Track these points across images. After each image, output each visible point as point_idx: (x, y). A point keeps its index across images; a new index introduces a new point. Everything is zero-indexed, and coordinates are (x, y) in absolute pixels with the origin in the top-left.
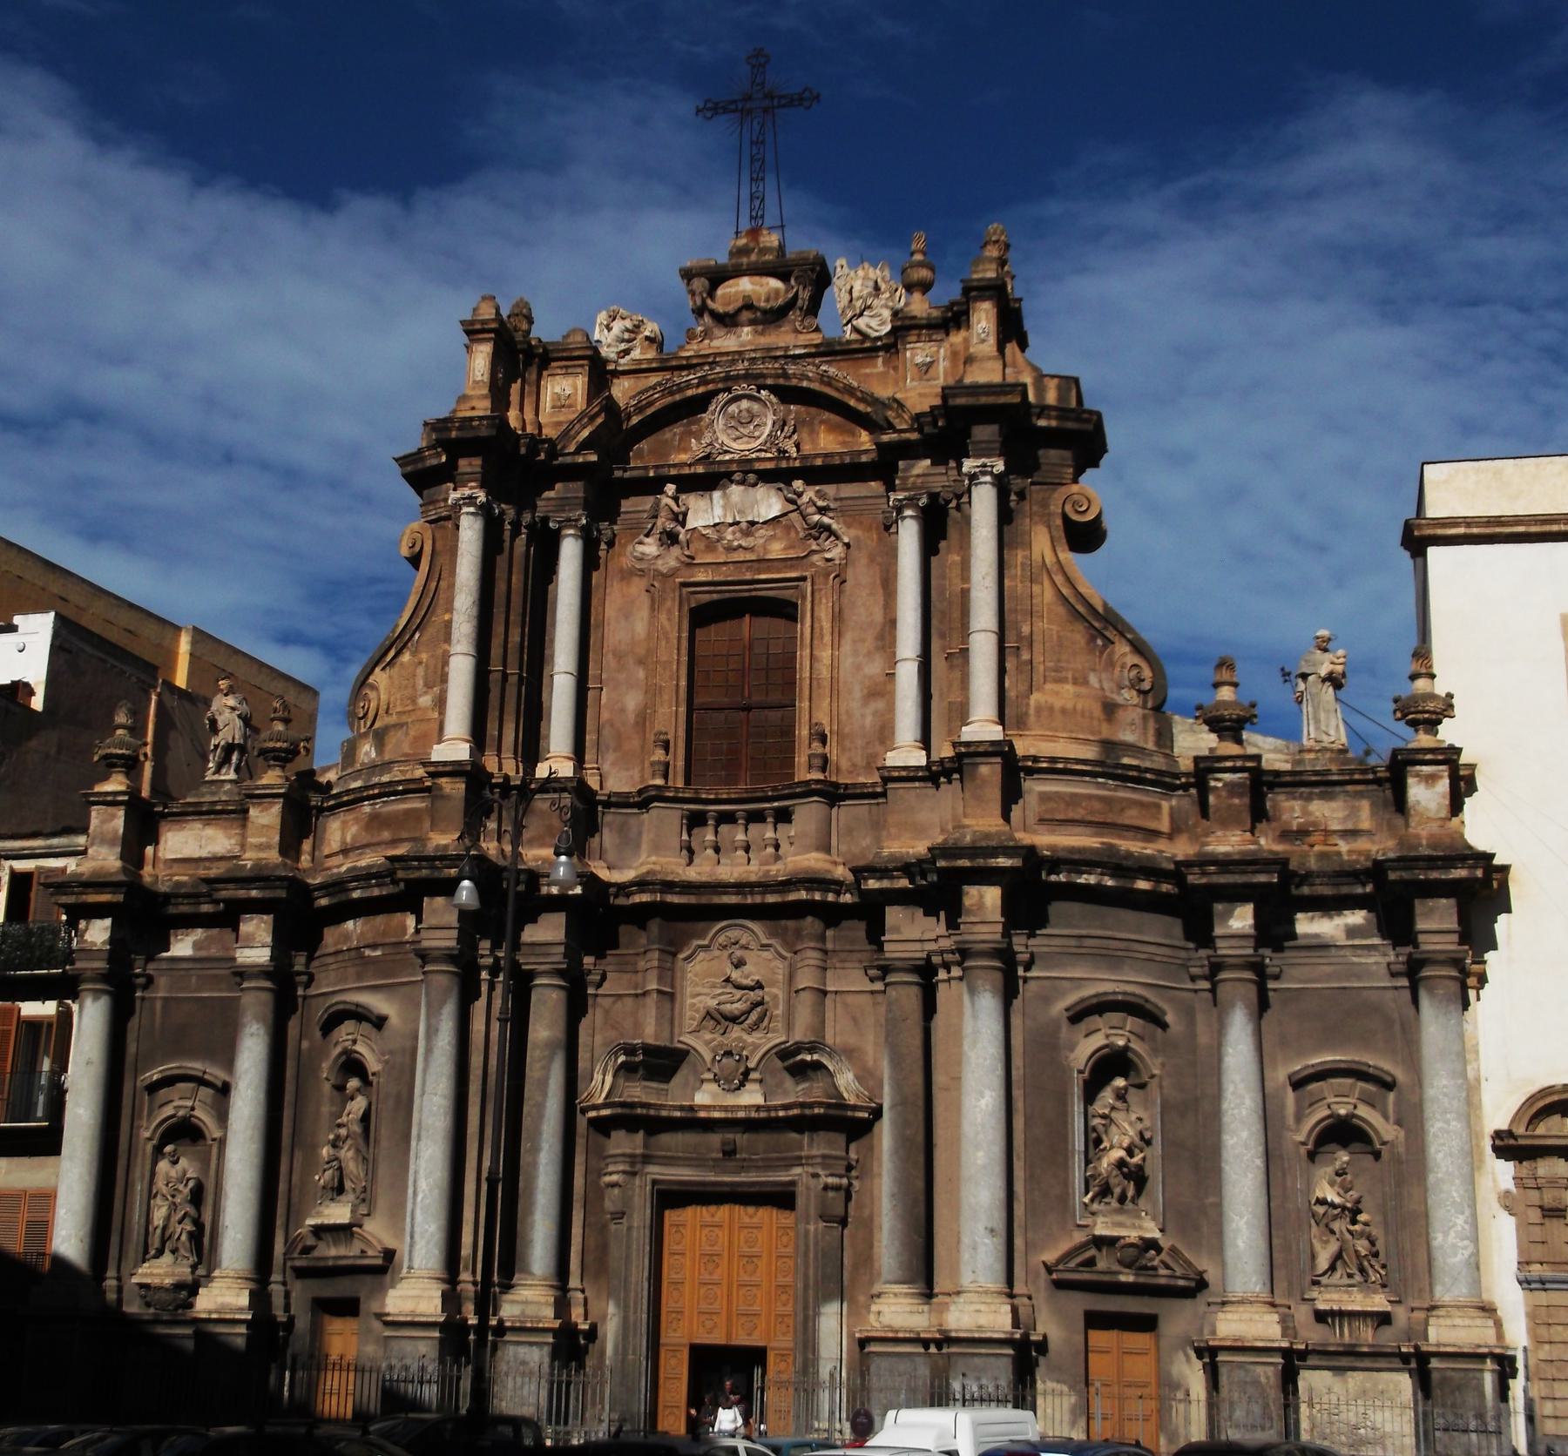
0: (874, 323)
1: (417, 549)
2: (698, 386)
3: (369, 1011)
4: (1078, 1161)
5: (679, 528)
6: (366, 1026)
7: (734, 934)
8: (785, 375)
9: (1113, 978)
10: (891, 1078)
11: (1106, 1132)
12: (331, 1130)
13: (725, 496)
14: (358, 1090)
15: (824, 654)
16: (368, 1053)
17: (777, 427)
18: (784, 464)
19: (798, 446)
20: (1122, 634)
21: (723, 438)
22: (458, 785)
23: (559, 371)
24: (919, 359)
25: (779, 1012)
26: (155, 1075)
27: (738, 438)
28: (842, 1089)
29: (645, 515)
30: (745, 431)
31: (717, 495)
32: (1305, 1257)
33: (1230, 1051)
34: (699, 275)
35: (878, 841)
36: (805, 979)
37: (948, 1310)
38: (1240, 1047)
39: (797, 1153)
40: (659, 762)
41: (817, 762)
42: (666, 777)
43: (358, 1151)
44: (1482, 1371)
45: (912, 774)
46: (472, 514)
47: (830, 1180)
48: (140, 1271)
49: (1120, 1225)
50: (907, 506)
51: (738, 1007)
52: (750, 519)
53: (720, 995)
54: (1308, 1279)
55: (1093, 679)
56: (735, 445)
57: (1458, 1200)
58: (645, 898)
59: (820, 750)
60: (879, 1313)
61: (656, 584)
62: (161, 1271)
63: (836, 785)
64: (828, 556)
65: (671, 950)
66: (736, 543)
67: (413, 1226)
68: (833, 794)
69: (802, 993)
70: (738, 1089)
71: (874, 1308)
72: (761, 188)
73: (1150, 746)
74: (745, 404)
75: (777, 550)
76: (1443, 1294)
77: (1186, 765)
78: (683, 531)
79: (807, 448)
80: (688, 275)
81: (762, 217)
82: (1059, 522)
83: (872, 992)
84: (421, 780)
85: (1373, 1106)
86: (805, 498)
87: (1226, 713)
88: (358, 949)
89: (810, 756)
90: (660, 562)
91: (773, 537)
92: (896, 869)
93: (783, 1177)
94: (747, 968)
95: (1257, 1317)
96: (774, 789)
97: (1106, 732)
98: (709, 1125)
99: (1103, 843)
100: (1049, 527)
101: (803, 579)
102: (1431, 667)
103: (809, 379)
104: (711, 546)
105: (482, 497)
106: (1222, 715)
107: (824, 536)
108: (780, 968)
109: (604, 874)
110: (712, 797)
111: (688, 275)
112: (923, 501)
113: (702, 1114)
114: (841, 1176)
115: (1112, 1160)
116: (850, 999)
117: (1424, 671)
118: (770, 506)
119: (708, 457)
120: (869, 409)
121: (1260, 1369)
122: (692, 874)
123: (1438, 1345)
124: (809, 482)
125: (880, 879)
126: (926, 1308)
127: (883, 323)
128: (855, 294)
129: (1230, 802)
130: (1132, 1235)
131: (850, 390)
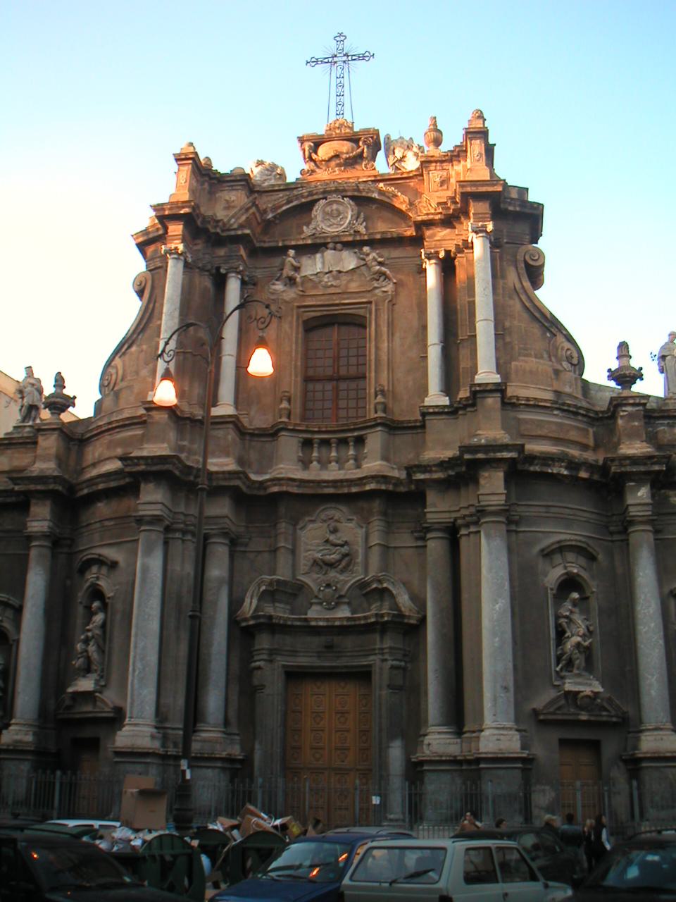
1: (143, 284)
2: (308, 196)
3: (107, 558)
4: (553, 643)
5: (296, 275)
6: (104, 570)
7: (331, 513)
8: (358, 190)
9: (568, 532)
11: (568, 627)
12: (83, 633)
13: (323, 257)
17: (354, 218)
18: (358, 238)
20: (560, 331)
21: (322, 225)
22: (163, 416)
23: (227, 188)
25: (360, 559)
27: (331, 225)
28: (401, 605)
31: (318, 256)
34: (308, 140)
35: (418, 455)
38: (647, 572)
39: (373, 647)
40: (285, 409)
41: (380, 407)
42: (289, 417)
43: (99, 646)
45: (441, 410)
49: (580, 684)
51: (335, 557)
52: (338, 269)
56: (329, 229)
58: (276, 489)
59: (383, 400)
60: (429, 744)
61: (282, 307)
63: (393, 421)
65: (294, 522)
66: (329, 284)
68: (393, 427)
69: (373, 548)
70: (333, 608)
73: (580, 396)
74: (335, 206)
75: (354, 287)
78: (298, 276)
80: (302, 140)
81: (343, 114)
82: (523, 265)
83: (417, 547)
84: (140, 417)
86: (371, 257)
87: (627, 372)
90: (284, 294)
91: (352, 280)
92: (435, 465)
93: (364, 662)
94: (339, 535)
95: (665, 738)
97: (556, 387)
98: (316, 631)
100: (517, 268)
101: (370, 303)
104: (315, 286)
106: (625, 374)
107: (382, 279)
108: (361, 532)
109: (253, 477)
111: (302, 140)
113: (313, 623)
114: (401, 661)
115: (573, 644)
116: (403, 551)
119: (314, 234)
125: (424, 472)
126: (459, 740)
130: (587, 690)
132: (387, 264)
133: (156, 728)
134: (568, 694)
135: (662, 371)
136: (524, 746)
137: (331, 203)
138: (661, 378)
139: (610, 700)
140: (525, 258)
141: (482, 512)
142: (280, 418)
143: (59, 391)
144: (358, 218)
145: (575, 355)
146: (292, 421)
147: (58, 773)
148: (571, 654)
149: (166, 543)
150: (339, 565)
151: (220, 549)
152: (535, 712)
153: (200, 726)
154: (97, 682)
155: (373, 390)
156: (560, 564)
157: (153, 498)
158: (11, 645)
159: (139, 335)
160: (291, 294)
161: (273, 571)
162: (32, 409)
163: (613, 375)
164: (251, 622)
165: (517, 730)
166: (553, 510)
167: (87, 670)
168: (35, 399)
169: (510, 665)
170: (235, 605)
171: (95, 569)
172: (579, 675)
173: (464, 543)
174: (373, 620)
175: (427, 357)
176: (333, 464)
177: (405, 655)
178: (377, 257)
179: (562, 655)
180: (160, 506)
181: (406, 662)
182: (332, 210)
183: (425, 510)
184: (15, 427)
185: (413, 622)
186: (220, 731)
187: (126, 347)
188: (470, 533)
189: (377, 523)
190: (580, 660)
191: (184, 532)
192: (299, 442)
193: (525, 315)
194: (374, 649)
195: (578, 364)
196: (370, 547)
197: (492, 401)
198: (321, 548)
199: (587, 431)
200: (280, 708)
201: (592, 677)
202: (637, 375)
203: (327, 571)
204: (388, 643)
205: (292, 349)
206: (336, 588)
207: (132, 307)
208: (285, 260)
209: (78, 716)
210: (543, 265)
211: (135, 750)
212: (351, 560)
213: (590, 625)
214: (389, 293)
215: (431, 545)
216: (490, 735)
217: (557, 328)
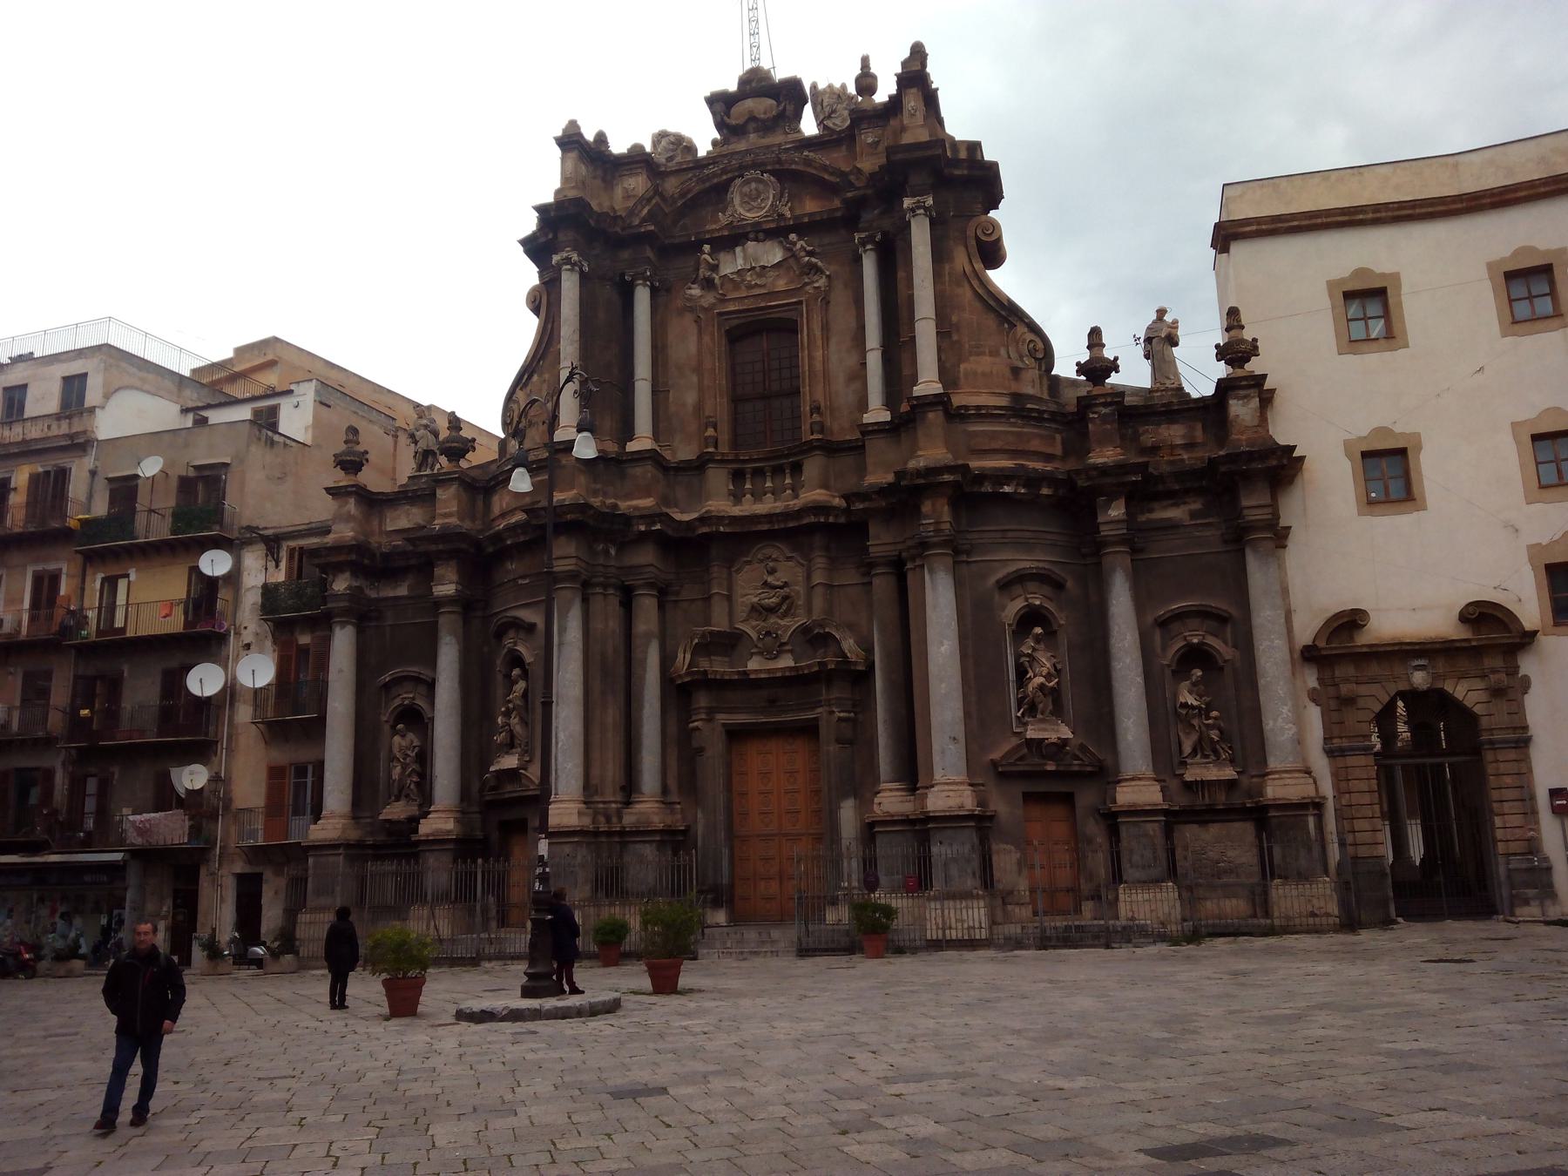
0: (838, 122)
2: (721, 174)
5: (714, 275)
6: (522, 635)
7: (768, 551)
8: (779, 161)
10: (878, 640)
13: (744, 251)
14: (519, 676)
15: (818, 354)
16: (526, 652)
19: (790, 209)
21: (741, 210)
23: (626, 173)
24: (870, 140)
26: (386, 678)
29: (691, 269)
30: (755, 204)
31: (738, 250)
32: (1174, 747)
33: (1114, 602)
36: (818, 578)
37: (927, 797)
41: (816, 428)
42: (716, 447)
43: (521, 719)
44: (1307, 815)
45: (881, 428)
46: (569, 270)
47: (842, 715)
48: (384, 811)
49: (1045, 730)
50: (868, 243)
53: (760, 594)
54: (1176, 760)
55: (1003, 352)
56: (748, 215)
57: (1282, 695)
58: (705, 530)
59: (818, 419)
62: (398, 810)
64: (816, 285)
66: (753, 283)
67: (556, 765)
68: (832, 449)
70: (775, 658)
71: (876, 801)
72: (757, 40)
73: (1046, 396)
74: (753, 185)
75: (781, 285)
76: (1273, 763)
77: (1072, 408)
79: (798, 212)
81: (759, 59)
82: (973, 242)
83: (863, 584)
85: (1216, 636)
86: (798, 246)
87: (1098, 365)
88: (514, 579)
89: (811, 424)
90: (703, 300)
96: (789, 448)
97: (1015, 387)
99: (1015, 464)
101: (800, 303)
102: (1240, 321)
103: (796, 163)
104: (736, 286)
105: (575, 257)
108: (800, 573)
109: (678, 517)
110: (747, 458)
112: (878, 238)
113: (752, 676)
114: (849, 712)
115: (1035, 685)
117: (1236, 324)
118: (775, 255)
120: (838, 180)
121: (1149, 826)
122: (736, 511)
123: (1274, 800)
124: (800, 237)
125: (863, 501)
126: (912, 797)
127: (844, 120)
128: (825, 104)
129: (1104, 427)
131: (825, 168)
132: (819, 253)
133: (585, 803)
134: (1030, 743)
135: (1147, 357)
136: (981, 803)
137: (748, 182)
138: (1146, 367)
139: (1083, 748)
140: (976, 233)
141: (924, 545)
142: (707, 448)
143: (454, 434)
144: (782, 196)
145: (1040, 345)
146: (719, 451)
147: (480, 861)
148: (1033, 698)
149: (585, 600)
150: (780, 609)
151: (647, 601)
152: (994, 764)
153: (635, 797)
154: (521, 755)
155: (808, 408)
156: (1021, 595)
157: (565, 554)
158: (427, 723)
159: (539, 361)
160: (709, 299)
161: (708, 622)
162: (425, 457)
163: (1081, 369)
164: (687, 679)
165: (971, 785)
166: (1010, 534)
167: (510, 746)
168: (430, 444)
169: (961, 714)
170: (666, 661)
171: (511, 633)
172: (1042, 721)
173: (910, 576)
174: (816, 669)
175: (866, 363)
176: (769, 495)
177: (854, 706)
178: (805, 246)
179: (1024, 698)
180: (573, 561)
181: (856, 713)
182: (751, 190)
183: (868, 543)
184: (409, 478)
185: (860, 668)
186: (657, 801)
187: (526, 377)
188: (916, 567)
189: (819, 560)
190: (1045, 704)
191: (605, 586)
192: (729, 472)
193: (978, 305)
194: (820, 701)
195: (1045, 355)
196: (813, 587)
197: (934, 417)
198: (760, 591)
199: (1054, 438)
200: (721, 771)
201: (1060, 722)
202: (1113, 366)
203: (767, 616)
204: (835, 694)
205: (715, 366)
206: (777, 634)
207: (530, 325)
208: (699, 258)
209: (507, 796)
210: (999, 239)
211: (561, 830)
212: (792, 603)
213: (1059, 663)
214: (823, 289)
215: (876, 581)
216: (938, 791)
217: (1017, 316)
